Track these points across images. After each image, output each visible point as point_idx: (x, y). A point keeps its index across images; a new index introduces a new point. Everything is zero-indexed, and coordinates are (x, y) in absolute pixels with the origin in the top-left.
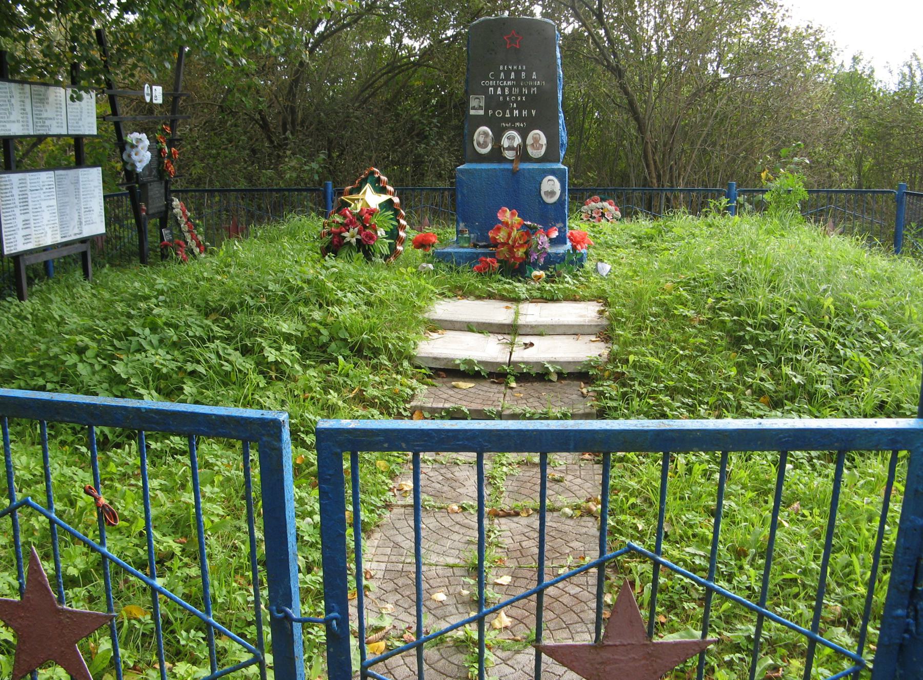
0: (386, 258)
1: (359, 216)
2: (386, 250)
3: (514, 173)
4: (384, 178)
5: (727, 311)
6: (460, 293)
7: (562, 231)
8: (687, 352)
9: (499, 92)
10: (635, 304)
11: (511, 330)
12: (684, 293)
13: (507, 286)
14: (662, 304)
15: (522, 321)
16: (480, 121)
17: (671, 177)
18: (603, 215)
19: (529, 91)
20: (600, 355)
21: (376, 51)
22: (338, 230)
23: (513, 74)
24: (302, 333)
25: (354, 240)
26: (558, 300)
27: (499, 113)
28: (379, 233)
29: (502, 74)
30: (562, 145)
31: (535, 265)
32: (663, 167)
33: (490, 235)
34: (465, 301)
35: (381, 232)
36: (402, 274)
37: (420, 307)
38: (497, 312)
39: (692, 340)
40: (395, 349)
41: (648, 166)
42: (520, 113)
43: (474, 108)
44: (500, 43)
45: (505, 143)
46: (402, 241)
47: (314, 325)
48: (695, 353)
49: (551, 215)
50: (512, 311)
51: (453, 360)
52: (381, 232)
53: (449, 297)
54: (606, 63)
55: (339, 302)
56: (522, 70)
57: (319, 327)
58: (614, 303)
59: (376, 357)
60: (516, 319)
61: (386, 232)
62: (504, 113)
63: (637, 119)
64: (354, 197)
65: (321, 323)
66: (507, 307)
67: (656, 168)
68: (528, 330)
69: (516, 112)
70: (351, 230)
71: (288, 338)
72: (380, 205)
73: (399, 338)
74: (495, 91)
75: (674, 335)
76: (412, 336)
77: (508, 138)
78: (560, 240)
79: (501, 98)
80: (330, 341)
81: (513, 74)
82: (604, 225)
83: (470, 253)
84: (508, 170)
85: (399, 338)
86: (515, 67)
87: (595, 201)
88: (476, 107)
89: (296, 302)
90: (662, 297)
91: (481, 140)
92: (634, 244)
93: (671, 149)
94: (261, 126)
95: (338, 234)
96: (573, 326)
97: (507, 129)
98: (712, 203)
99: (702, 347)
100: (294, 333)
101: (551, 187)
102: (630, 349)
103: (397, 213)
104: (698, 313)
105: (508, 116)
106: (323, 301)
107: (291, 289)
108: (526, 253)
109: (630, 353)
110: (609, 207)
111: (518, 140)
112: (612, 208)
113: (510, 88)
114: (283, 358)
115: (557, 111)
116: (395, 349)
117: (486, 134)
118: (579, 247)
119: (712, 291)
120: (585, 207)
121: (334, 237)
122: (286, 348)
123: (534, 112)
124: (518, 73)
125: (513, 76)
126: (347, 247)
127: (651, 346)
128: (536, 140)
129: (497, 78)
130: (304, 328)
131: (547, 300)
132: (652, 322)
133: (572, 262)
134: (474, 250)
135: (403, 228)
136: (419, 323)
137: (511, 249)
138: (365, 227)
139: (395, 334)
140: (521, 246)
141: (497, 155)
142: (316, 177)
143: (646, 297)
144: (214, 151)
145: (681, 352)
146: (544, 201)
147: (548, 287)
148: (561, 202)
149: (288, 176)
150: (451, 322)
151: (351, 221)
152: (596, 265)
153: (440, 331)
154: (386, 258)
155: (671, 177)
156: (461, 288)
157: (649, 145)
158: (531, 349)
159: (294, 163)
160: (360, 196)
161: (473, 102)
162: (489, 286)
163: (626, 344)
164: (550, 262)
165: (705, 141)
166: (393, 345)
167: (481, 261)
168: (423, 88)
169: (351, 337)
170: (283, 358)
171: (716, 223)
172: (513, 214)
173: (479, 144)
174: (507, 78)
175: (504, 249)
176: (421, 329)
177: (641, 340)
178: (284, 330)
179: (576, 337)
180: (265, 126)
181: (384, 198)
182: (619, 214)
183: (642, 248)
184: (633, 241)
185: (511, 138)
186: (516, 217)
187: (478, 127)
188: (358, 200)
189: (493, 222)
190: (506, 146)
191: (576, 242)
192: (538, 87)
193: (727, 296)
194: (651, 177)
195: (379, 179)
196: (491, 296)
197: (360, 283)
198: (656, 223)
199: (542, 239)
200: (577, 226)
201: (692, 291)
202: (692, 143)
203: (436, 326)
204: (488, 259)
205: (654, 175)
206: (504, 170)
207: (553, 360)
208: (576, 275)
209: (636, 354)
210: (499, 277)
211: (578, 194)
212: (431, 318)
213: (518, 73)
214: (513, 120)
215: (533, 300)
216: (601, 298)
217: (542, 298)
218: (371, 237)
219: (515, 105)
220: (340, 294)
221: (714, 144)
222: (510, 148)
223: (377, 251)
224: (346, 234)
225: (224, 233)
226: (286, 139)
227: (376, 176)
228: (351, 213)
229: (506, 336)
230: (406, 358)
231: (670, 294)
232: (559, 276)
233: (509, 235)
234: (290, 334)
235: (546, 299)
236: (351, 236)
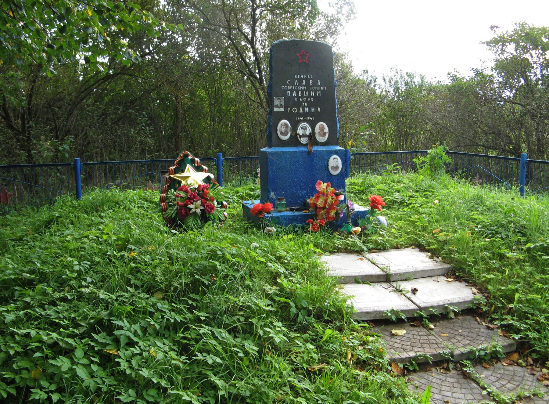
9: (294, 94)
19: (315, 94)
23: (304, 81)
25: (198, 211)
27: (295, 110)
29: (296, 81)
42: (310, 110)
43: (276, 106)
45: (300, 132)
56: (310, 79)
62: (299, 110)
68: (398, 278)
69: (307, 109)
74: (292, 93)
79: (296, 99)
81: (304, 81)
86: (305, 77)
91: (283, 130)
96: (427, 271)
97: (300, 122)
113: (302, 91)
117: (286, 125)
123: (319, 109)
124: (307, 80)
125: (304, 82)
128: (322, 129)
129: (293, 84)
141: (294, 140)
146: (330, 174)
173: (281, 133)
174: (300, 84)
181: (204, 175)
185: (304, 128)
187: (280, 120)
190: (301, 134)
192: (321, 91)
206: (302, 152)
213: (307, 80)
214: (305, 115)
217: (375, 249)
219: (306, 104)
222: (304, 136)
223: (217, 218)
224: (191, 206)
233: (326, 201)
235: (380, 249)
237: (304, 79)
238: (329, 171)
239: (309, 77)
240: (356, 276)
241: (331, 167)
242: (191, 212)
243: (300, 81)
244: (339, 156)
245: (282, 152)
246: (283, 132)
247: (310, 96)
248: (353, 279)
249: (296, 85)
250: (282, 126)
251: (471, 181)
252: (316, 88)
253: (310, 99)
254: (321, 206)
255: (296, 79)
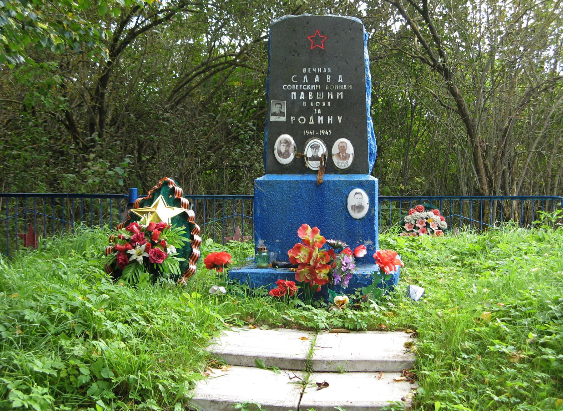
0: (176, 278)
1: (148, 232)
2: (176, 269)
3: (318, 185)
4: (179, 189)
5: (552, 347)
6: (252, 321)
7: (371, 249)
8: (503, 398)
9: (302, 96)
10: (447, 337)
11: (306, 366)
12: (502, 325)
13: (305, 313)
14: (477, 338)
15: (318, 355)
16: (281, 129)
17: (504, 182)
18: (428, 225)
19: (335, 96)
20: (403, 399)
21: (192, 51)
22: (124, 247)
23: (317, 77)
24: (59, 371)
25: (140, 259)
26: (361, 330)
27: (302, 120)
28: (169, 251)
29: (306, 77)
30: (371, 154)
31: (338, 289)
32: (495, 172)
33: (290, 255)
34: (257, 330)
35: (172, 250)
36: (186, 300)
37: (202, 339)
38: (289, 344)
39: (509, 383)
40: (167, 390)
41: (478, 171)
42: (325, 120)
43: (275, 114)
44: (308, 42)
45: (309, 152)
46: (196, 260)
47: (72, 362)
48: (513, 400)
49: (359, 232)
50: (307, 343)
51: (234, 404)
52: (172, 250)
53: (239, 326)
54: (432, 63)
55: (107, 335)
57: (78, 363)
58: (424, 335)
59: (144, 401)
60: (310, 354)
61: (178, 250)
62: (308, 120)
63: (466, 121)
64: (145, 209)
65: (82, 360)
66: (303, 338)
67: (487, 173)
68: (325, 367)
69: (321, 119)
70: (138, 247)
71: (40, 379)
72: (173, 219)
73: (173, 378)
75: (489, 377)
76: (189, 374)
77: (312, 147)
78: (369, 260)
80: (92, 380)
81: (317, 77)
82: (425, 239)
83: (267, 274)
84: (312, 182)
85: (173, 378)
86: (320, 70)
87: (420, 211)
88: (277, 113)
89: (57, 334)
90: (477, 329)
91: (283, 149)
92: (455, 261)
93: (503, 153)
94: (67, 126)
95: (124, 252)
96: (375, 362)
98: (544, 214)
99: (522, 391)
100: (48, 372)
101: (359, 200)
102: (437, 393)
103: (190, 228)
104: (519, 349)
105: (312, 122)
106: (90, 331)
107: (52, 319)
108: (329, 275)
109: (437, 398)
110: (435, 217)
111: (322, 150)
112: (438, 218)
113: (314, 92)
114: (31, 403)
115: (365, 118)
116: (167, 390)
117: (287, 142)
118: (387, 269)
119: (535, 322)
120: (409, 217)
121: (119, 255)
122: (38, 390)
123: (340, 119)
124: (322, 76)
126: (134, 266)
127: (461, 390)
128: (343, 149)
129: (299, 81)
130: (62, 366)
131: (348, 330)
132: (464, 359)
133: (380, 285)
134: (273, 271)
135: (197, 244)
136: (199, 358)
137: (312, 271)
138: (153, 244)
139: (167, 373)
140: (324, 266)
141: (299, 165)
142: (121, 183)
143: (458, 330)
144: (14, 152)
145: (496, 398)
146: (351, 217)
147: (350, 313)
148: (369, 217)
149: (90, 181)
150: (237, 356)
151: (138, 237)
152: (408, 288)
153: (224, 367)
154: (176, 278)
155: (504, 182)
156: (253, 315)
157: (479, 149)
158: (325, 389)
159: (97, 167)
160: (151, 209)
161: (274, 108)
162: (286, 314)
163: (433, 386)
164: (356, 283)
165: (540, 143)
166: (164, 386)
167: (279, 284)
168: (242, 90)
169: (116, 376)
170: (31, 403)
171: (547, 237)
172: (314, 232)
173: (280, 153)
174: (311, 82)
175: (305, 270)
176: (203, 364)
177: (451, 382)
178: (36, 369)
179: (377, 375)
180: (71, 127)
181: (178, 211)
182: (444, 225)
183: (463, 265)
184: (454, 257)
185: (315, 147)
186: (318, 235)
187: (279, 135)
188: (147, 213)
189: (293, 242)
190: (309, 155)
191: (384, 263)
192: (344, 91)
193: (552, 329)
194: (482, 184)
195: (173, 191)
196: (286, 325)
197: (136, 311)
198: (481, 237)
199: (347, 259)
200: (391, 241)
201: (511, 322)
202: (528, 146)
203: (218, 361)
204: (286, 282)
205: (485, 181)
206: (307, 182)
207: (348, 404)
208: (385, 300)
209: (443, 399)
210: (298, 302)
211: (397, 202)
212: (215, 351)
213: (322, 76)
214: (317, 127)
215: (333, 329)
216: (409, 327)
218: (159, 255)
219: (319, 111)
220: (109, 324)
221: (551, 147)
222: (314, 158)
224: (132, 252)
225: (20, 241)
226: (93, 140)
227: (171, 186)
228: (139, 228)
229: (298, 374)
230: (179, 401)
231: (487, 326)
232: (365, 301)
233: (310, 254)
234: (44, 374)
236: (137, 253)
237: (317, 73)
238: (348, 212)
239: (325, 70)
240: (258, 357)
241: (352, 207)
242: (131, 259)
243: (311, 77)
244: (365, 190)
245: (276, 182)
246: (283, 151)
247: (326, 99)
248: (253, 361)
249: (305, 83)
250: (281, 143)
251: (487, 230)
252: (336, 87)
253: (327, 104)
254: (303, 261)
255: (305, 74)
